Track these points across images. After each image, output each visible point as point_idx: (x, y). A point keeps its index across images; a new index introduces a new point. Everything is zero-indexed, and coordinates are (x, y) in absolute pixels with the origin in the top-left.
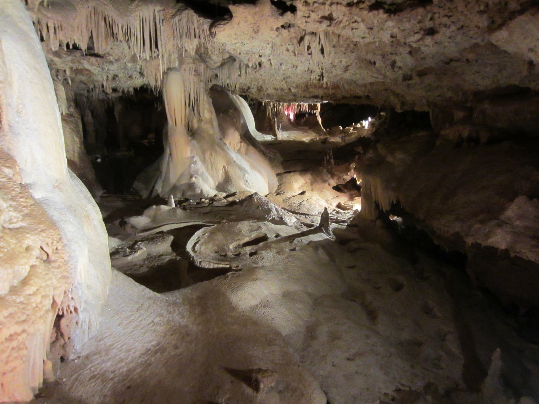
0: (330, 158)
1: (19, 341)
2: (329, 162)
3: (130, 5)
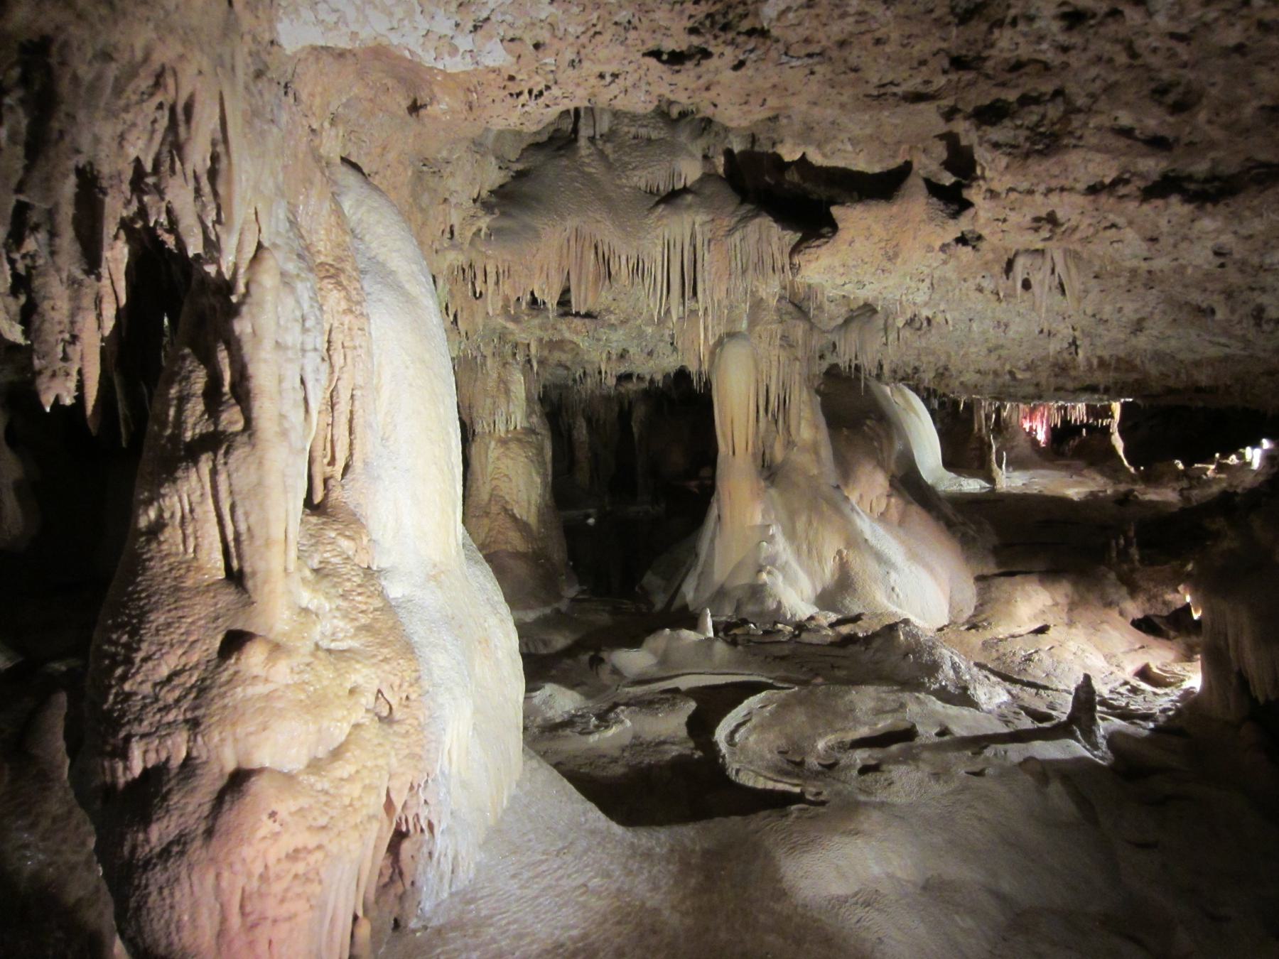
0: (1128, 543)
1: (308, 864)
2: (1124, 554)
3: (646, 216)
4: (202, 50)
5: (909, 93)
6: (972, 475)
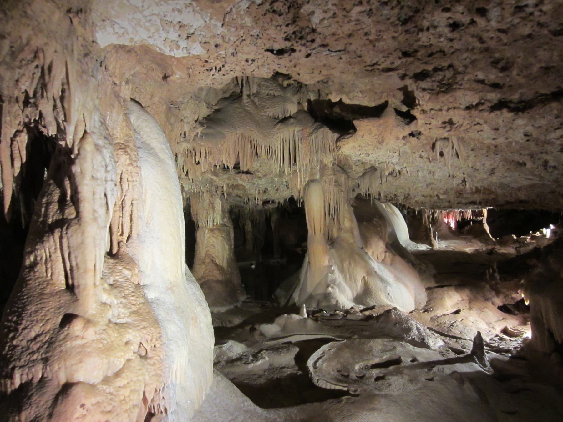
0: (494, 271)
2: (492, 277)
4: (56, 41)
5: (385, 68)
6: (423, 243)
